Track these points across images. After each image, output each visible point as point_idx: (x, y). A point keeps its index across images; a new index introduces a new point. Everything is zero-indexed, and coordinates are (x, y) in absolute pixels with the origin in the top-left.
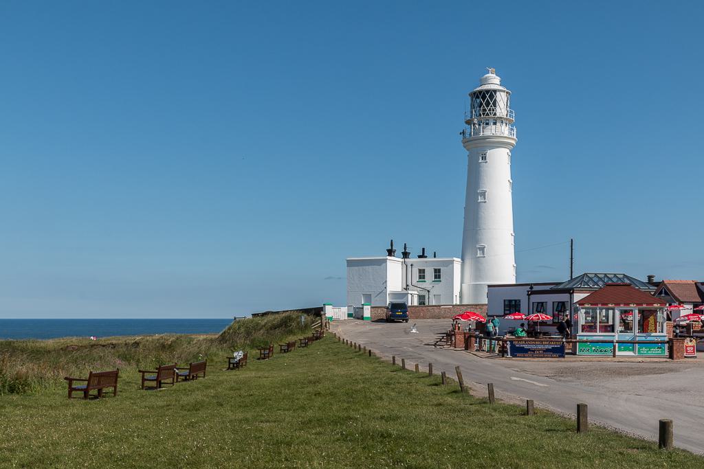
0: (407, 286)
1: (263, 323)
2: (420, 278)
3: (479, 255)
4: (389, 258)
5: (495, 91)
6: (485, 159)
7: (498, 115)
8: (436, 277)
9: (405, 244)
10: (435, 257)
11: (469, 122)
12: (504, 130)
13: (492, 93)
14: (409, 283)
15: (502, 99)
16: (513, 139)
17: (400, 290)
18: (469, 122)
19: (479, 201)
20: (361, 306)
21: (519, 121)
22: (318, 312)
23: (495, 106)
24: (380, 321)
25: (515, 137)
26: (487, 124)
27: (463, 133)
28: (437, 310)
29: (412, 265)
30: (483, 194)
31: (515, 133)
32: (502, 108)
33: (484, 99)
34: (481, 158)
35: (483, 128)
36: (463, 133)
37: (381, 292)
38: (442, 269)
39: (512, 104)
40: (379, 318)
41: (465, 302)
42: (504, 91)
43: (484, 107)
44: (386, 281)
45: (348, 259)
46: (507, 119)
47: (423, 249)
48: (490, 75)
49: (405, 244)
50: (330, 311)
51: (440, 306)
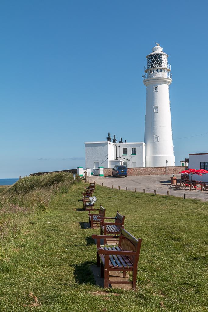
0: (117, 157)
1: (42, 179)
2: (124, 153)
3: (155, 141)
4: (108, 142)
5: (161, 55)
6: (157, 90)
7: (163, 67)
8: (133, 153)
9: (109, 133)
10: (126, 142)
11: (146, 71)
12: (164, 75)
13: (160, 56)
14: (118, 156)
15: (164, 58)
16: (171, 80)
17: (113, 160)
18: (146, 71)
19: (154, 112)
20: (98, 169)
21: (173, 71)
22: (75, 171)
23: (161, 62)
24: (109, 176)
25: (171, 79)
26: (158, 71)
27: (144, 76)
28: (138, 170)
29: (119, 146)
30: (157, 108)
31: (171, 76)
32: (164, 64)
33: (154, 59)
34: (154, 89)
35: (156, 74)
36: (144, 76)
37: (104, 161)
38: (136, 148)
39: (169, 62)
40: (109, 175)
41: (148, 166)
42: (166, 55)
43: (155, 63)
44: (108, 155)
45: (86, 143)
46: (167, 69)
47: (121, 138)
48: (157, 46)
49: (109, 133)
50: (81, 172)
51: (140, 168)
